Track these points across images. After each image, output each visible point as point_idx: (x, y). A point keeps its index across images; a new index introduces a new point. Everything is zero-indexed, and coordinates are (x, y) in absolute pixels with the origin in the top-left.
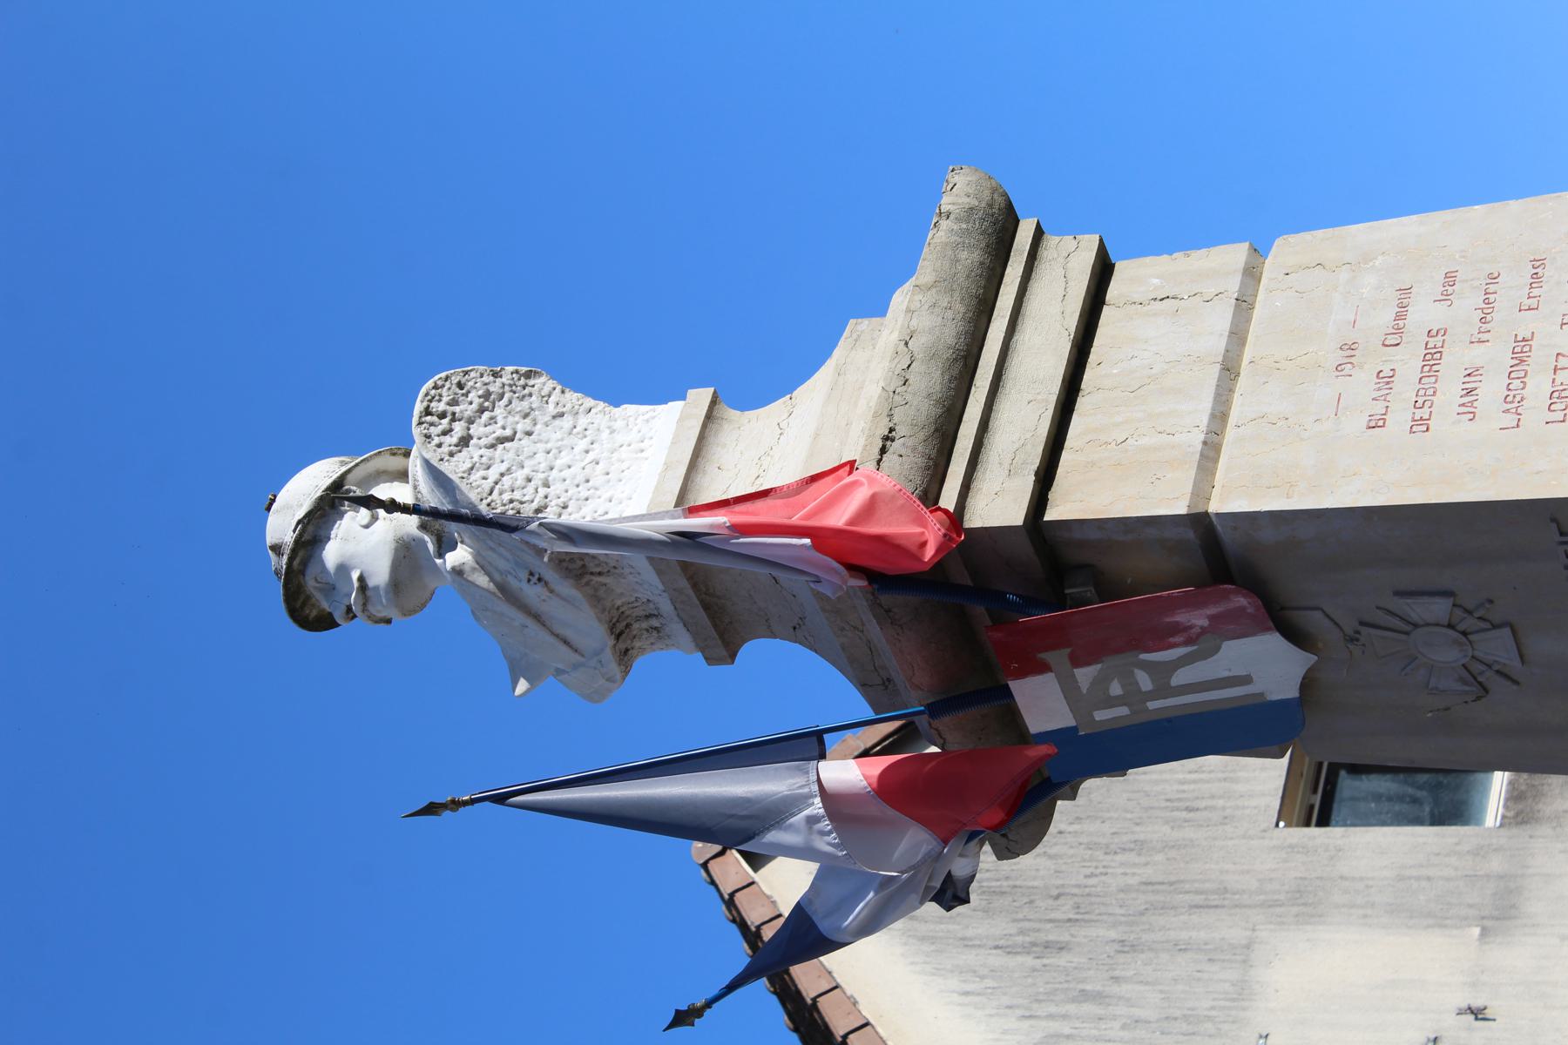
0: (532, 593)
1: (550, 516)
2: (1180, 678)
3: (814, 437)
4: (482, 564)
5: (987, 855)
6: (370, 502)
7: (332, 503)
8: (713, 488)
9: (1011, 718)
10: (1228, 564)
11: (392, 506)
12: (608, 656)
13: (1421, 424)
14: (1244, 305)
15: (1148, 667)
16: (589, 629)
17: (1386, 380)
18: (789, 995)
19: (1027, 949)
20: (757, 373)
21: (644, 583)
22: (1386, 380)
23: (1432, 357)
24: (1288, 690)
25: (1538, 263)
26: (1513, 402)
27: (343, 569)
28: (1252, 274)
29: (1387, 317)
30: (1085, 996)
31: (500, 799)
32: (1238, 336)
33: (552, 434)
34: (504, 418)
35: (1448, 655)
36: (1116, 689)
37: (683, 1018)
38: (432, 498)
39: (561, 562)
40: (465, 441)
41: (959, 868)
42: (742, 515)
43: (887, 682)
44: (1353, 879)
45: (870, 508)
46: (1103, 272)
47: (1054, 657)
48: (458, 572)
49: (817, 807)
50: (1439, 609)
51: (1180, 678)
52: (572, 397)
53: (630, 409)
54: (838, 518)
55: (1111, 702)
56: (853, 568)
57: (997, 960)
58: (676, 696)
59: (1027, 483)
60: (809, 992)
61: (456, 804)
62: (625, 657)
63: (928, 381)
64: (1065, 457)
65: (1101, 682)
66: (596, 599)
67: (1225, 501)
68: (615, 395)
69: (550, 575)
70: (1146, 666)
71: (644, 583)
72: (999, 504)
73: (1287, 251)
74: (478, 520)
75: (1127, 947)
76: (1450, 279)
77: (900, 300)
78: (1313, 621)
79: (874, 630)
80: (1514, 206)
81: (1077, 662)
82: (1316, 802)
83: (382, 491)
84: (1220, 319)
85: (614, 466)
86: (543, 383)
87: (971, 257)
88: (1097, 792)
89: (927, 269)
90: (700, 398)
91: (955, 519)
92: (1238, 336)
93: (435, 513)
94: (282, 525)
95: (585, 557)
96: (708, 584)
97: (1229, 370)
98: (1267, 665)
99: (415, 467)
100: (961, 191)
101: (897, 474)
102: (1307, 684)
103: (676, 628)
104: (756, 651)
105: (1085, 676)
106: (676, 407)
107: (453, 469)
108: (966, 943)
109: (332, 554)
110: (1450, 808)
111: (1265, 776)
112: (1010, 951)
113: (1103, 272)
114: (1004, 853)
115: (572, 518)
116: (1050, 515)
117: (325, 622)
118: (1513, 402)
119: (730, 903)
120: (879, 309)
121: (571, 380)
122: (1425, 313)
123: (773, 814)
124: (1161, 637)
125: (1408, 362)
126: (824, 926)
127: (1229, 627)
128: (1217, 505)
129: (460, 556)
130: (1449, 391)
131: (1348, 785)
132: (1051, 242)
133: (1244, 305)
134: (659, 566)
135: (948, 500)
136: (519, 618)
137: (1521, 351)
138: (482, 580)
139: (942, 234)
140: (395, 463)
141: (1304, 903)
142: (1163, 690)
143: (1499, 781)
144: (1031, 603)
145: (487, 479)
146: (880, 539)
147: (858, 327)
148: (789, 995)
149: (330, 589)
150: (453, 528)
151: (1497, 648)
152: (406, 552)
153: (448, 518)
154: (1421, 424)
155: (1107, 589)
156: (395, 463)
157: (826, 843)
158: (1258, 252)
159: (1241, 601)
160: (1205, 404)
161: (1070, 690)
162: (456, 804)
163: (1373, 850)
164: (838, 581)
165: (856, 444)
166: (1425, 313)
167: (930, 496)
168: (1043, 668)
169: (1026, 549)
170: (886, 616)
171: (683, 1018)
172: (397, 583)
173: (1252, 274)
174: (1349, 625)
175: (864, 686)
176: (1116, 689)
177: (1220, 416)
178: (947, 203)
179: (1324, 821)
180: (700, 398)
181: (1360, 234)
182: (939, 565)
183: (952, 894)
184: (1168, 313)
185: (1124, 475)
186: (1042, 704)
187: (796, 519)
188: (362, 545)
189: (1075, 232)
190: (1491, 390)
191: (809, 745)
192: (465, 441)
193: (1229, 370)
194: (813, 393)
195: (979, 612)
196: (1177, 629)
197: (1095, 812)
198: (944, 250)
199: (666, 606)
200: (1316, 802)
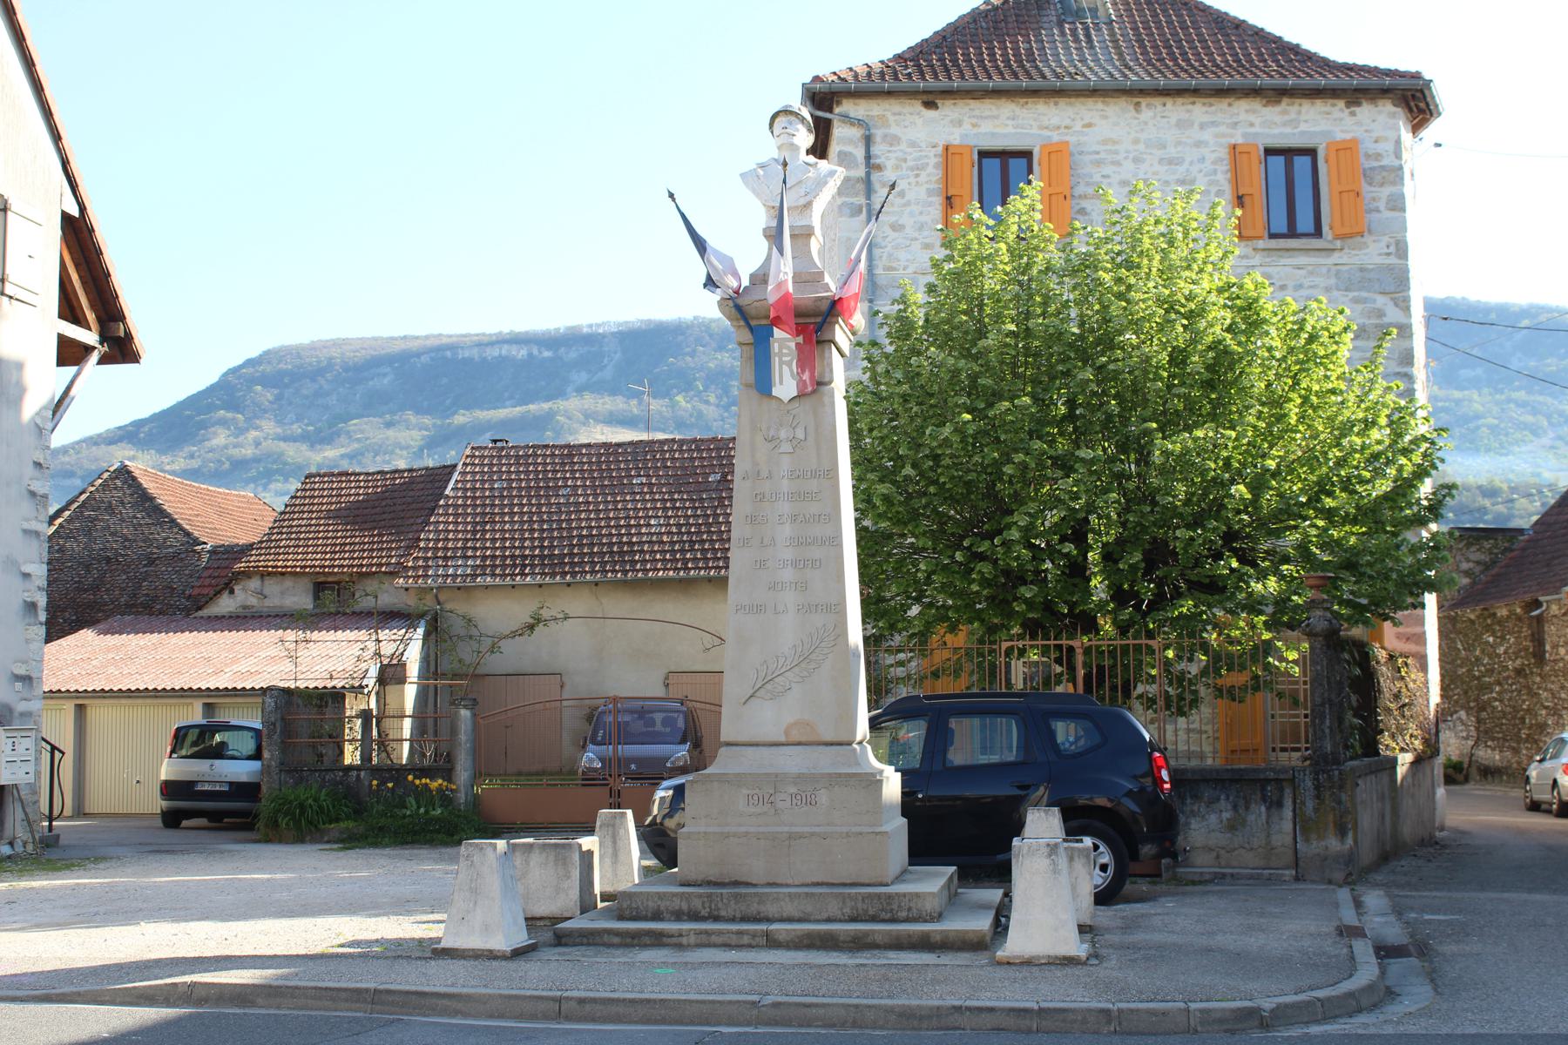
55: (780, 349)
142: (781, 363)
151: (786, 447)
171: (671, 196)
196: (803, 371)
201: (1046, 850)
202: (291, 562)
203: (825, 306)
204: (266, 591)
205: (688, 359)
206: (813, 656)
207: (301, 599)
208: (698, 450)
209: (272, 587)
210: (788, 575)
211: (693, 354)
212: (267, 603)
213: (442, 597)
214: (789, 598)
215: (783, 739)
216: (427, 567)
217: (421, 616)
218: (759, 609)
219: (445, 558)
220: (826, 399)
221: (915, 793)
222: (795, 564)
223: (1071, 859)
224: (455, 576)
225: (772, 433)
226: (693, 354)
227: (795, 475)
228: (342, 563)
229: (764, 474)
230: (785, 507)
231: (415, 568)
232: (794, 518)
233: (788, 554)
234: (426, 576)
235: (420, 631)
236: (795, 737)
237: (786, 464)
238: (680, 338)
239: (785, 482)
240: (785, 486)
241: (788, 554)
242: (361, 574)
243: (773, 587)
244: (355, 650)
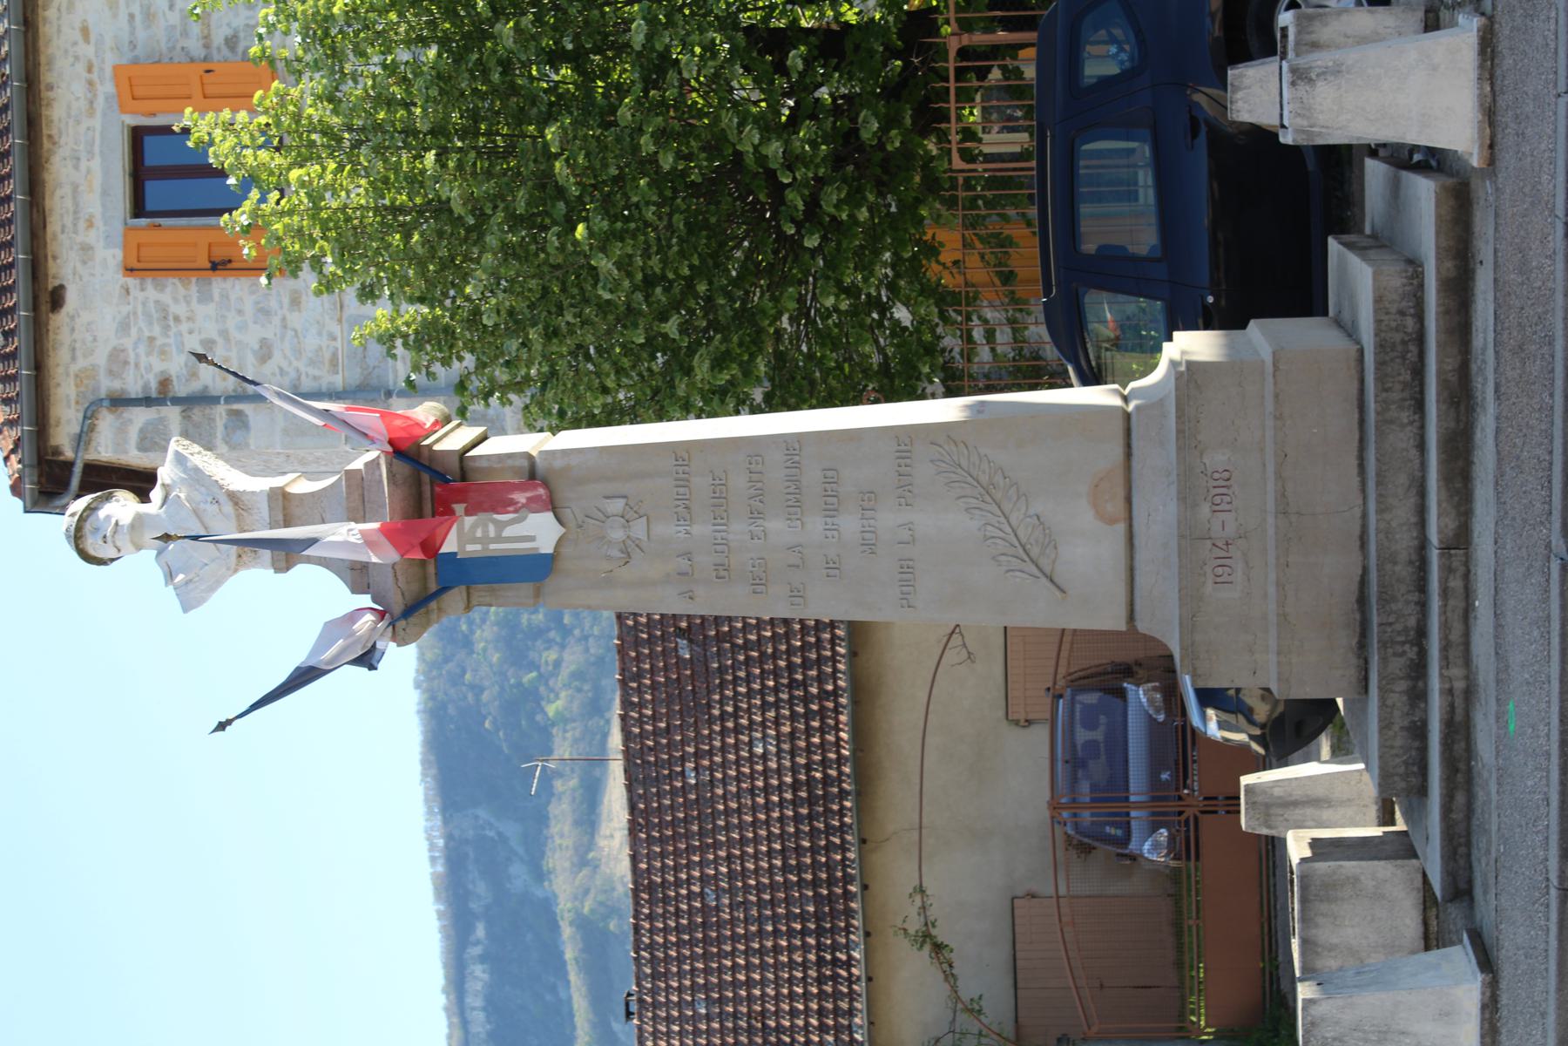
2: (507, 532)
51: (507, 532)
55: (475, 541)
65: (474, 527)
70: (495, 522)
78: (567, 514)
142: (499, 539)
169: (455, 464)
196: (512, 503)
201: (1302, 88)
205: (485, 696)
206: (984, 479)
208: (638, 676)
210: (849, 524)
211: (478, 689)
214: (888, 519)
215: (1121, 527)
218: (907, 569)
221: (1205, 307)
222: (831, 511)
223: (1315, 46)
225: (615, 553)
226: (478, 689)
227: (685, 513)
229: (683, 564)
230: (738, 529)
232: (755, 515)
233: (815, 525)
237: (667, 529)
238: (451, 710)
239: (696, 529)
240: (702, 529)
241: (815, 525)
243: (869, 546)
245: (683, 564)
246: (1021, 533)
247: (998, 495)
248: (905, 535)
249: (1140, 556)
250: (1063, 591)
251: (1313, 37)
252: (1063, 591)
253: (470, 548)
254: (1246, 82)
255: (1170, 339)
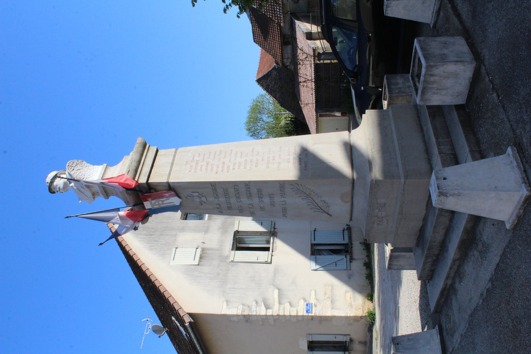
0: (82, 190)
1: (84, 180)
2: (165, 202)
3: (120, 171)
4: (75, 186)
5: (140, 223)
6: (59, 177)
7: (56, 177)
8: (107, 176)
9: (144, 207)
10: (171, 189)
11: (63, 178)
12: (92, 198)
13: (195, 172)
14: (174, 156)
15: (161, 201)
16: (89, 194)
17: (191, 166)
18: (118, 241)
19: (148, 235)
20: (112, 162)
21: (97, 189)
22: (191, 166)
23: (197, 163)
24: (178, 204)
25: (210, 153)
26: (206, 169)
27: (56, 186)
28: (176, 152)
29: (191, 158)
30: (155, 241)
31: (76, 216)
32: (174, 160)
33: (86, 169)
34: (79, 167)
35: (198, 200)
36: (157, 203)
37: (101, 244)
38: (69, 177)
39: (86, 186)
40: (73, 170)
41: (137, 226)
42: (110, 180)
43: (128, 202)
44: (425, 219)
45: (126, 180)
46: (157, 151)
47: (150, 199)
48: (72, 186)
49: (118, 217)
50: (197, 194)
51: (165, 202)
52: (88, 164)
53: (96, 166)
54: (122, 181)
55: (156, 205)
56: (124, 187)
57: (144, 236)
58: (101, 202)
59: (146, 178)
60: (120, 241)
61: (71, 217)
62: (94, 198)
63: (135, 164)
64: (151, 174)
65: (155, 203)
66: (90, 190)
67: (171, 181)
68: (94, 164)
69: (84, 187)
70: (161, 201)
71: (97, 189)
72: (143, 180)
73: (180, 150)
74: (74, 180)
75: (161, 235)
76: (199, 154)
77: (131, 153)
78: (182, 195)
79: (126, 195)
80: (207, 146)
81: (152, 200)
82: (185, 217)
83: (62, 176)
84: (171, 158)
85: (94, 174)
86: (84, 162)
87: (141, 149)
88: (154, 216)
89: (135, 150)
90: (105, 165)
91: (137, 182)
92: (174, 160)
93: (68, 179)
94: (48, 180)
95: (89, 185)
96: (105, 189)
97: (172, 164)
98: (176, 201)
99: (67, 173)
100: (140, 140)
101: (130, 175)
102: (181, 203)
103: (101, 194)
104: (112, 198)
105: (153, 202)
106: (102, 166)
107: (72, 173)
108: (141, 234)
109: (55, 184)
110: (201, 218)
111: (179, 213)
112: (146, 235)
113: (157, 151)
114: (143, 224)
115: (87, 180)
116: (149, 181)
117: (54, 193)
118: (206, 169)
119: (110, 229)
120: (128, 154)
121: (88, 162)
122: (196, 158)
123: (112, 218)
124: (163, 197)
125: (194, 164)
126: (119, 233)
127: (171, 196)
128: (170, 181)
129: (72, 184)
130: (199, 168)
131: (189, 215)
132: (151, 147)
133: (174, 156)
134: (99, 187)
135: (136, 179)
136: (80, 193)
137: (224, 163)
138: (75, 188)
139: (137, 146)
140: (64, 172)
141: (183, 230)
142: (163, 204)
143: (207, 215)
144: (146, 193)
145: (76, 175)
146: (127, 184)
147: (126, 157)
148: (118, 241)
149: (55, 188)
150: (72, 181)
151: (204, 199)
152: (65, 184)
153: (71, 180)
154: (195, 172)
155: (156, 191)
156: (64, 172)
157: (119, 222)
158: (177, 150)
159: (173, 193)
160: (169, 168)
161: (151, 204)
162: (71, 217)
163: (192, 223)
164: (121, 189)
165: (125, 172)
166: (196, 158)
167: (134, 179)
168: (148, 201)
169: (146, 185)
170: (128, 194)
171: (101, 244)
172: (64, 188)
173: (176, 152)
174: (186, 196)
175: (125, 202)
176: (157, 203)
177: (171, 170)
178: (138, 142)
179: (186, 219)
180: (105, 165)
181: (189, 148)
182: (135, 187)
183: (136, 229)
184: (165, 157)
185: (159, 177)
186: (148, 205)
187: (117, 181)
188: (59, 183)
189: (154, 146)
190: (204, 168)
191: (118, 210)
192: (73, 170)
193: (172, 164)
194: (120, 165)
195: (140, 193)
196: (165, 196)
197: (153, 219)
198: (137, 147)
199: (99, 191)
200: (185, 217)
201: (442, 198)
202: (279, 52)
203: (129, 192)
204: (287, 57)
206: (308, 193)
207: (289, 49)
209: (286, 56)
212: (290, 57)
213: (286, 12)
215: (349, 204)
216: (277, 16)
217: (291, 19)
219: (274, 11)
220: (176, 185)
221: (369, 37)
223: (432, 75)
224: (279, 9)
228: (278, 39)
229: (218, 206)
231: (278, 20)
234: (280, 17)
235: (296, 21)
236: (349, 199)
242: (281, 32)
244: (305, 89)
245: (218, 206)
246: (319, 204)
247: (312, 197)
248: (284, 203)
249: (355, 210)
250: (331, 216)
251: (432, 73)
252: (331, 216)
253: (155, 207)
254: (392, 5)
255: (364, 113)
